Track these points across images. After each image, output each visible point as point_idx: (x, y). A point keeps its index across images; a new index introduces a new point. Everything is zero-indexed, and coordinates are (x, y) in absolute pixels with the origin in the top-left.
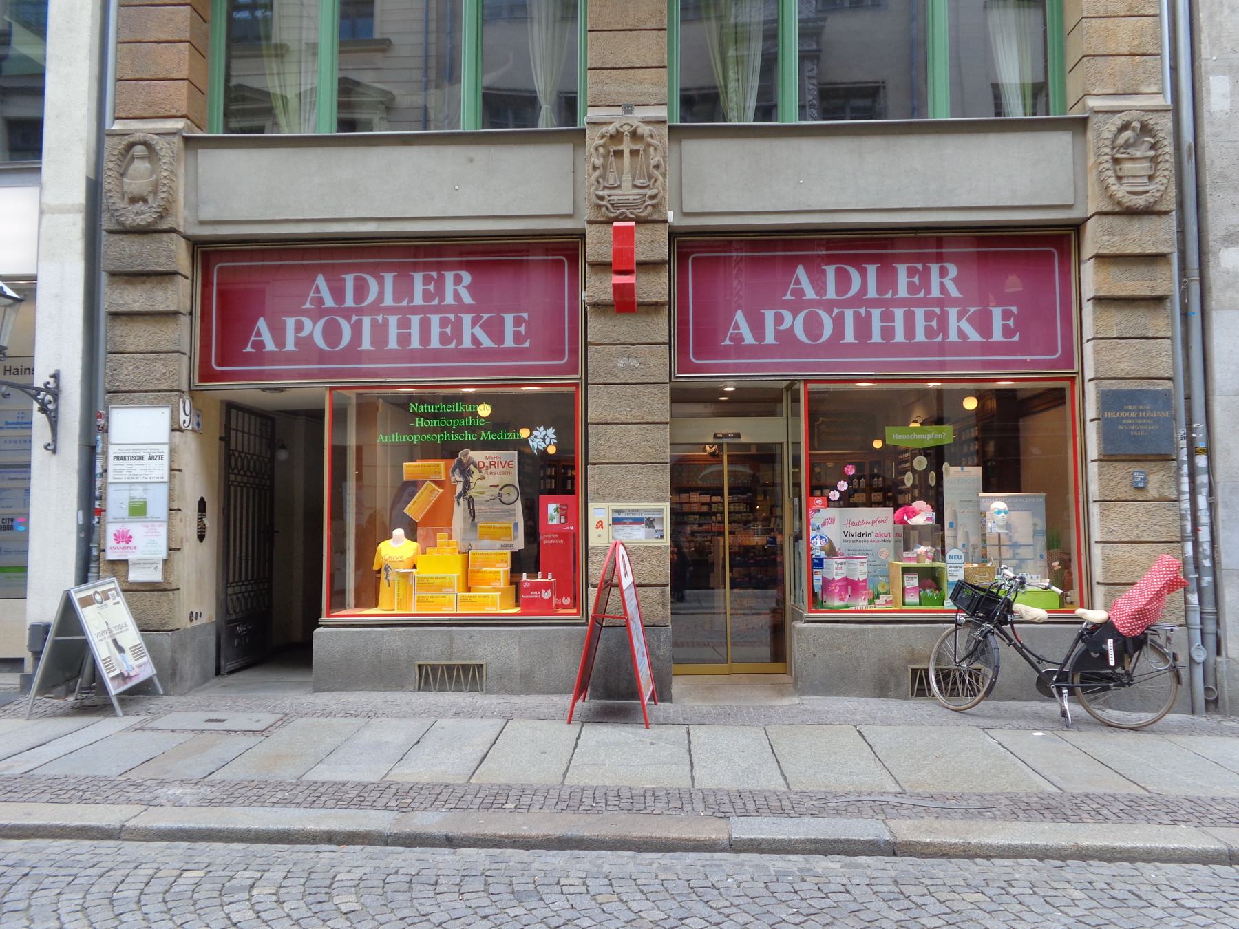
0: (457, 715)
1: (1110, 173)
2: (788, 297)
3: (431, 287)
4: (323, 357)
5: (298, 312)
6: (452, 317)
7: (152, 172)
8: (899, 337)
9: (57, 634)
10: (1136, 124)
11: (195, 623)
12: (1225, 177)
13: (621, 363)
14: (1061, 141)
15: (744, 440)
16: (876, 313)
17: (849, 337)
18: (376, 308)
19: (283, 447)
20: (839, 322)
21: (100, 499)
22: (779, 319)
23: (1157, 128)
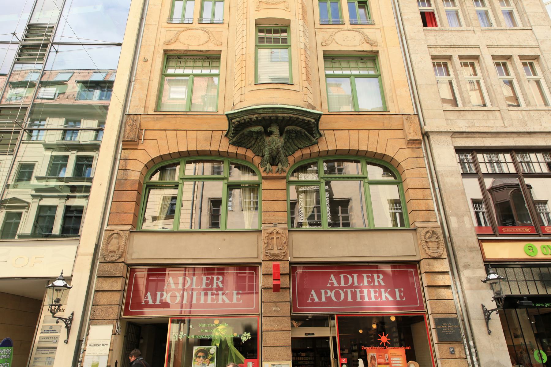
2: (329, 285)
5: (326, 288)
12: (460, 247)
13: (274, 309)
15: (316, 336)
16: (358, 291)
17: (350, 299)
19: (142, 338)
21: (81, 362)
22: (326, 293)
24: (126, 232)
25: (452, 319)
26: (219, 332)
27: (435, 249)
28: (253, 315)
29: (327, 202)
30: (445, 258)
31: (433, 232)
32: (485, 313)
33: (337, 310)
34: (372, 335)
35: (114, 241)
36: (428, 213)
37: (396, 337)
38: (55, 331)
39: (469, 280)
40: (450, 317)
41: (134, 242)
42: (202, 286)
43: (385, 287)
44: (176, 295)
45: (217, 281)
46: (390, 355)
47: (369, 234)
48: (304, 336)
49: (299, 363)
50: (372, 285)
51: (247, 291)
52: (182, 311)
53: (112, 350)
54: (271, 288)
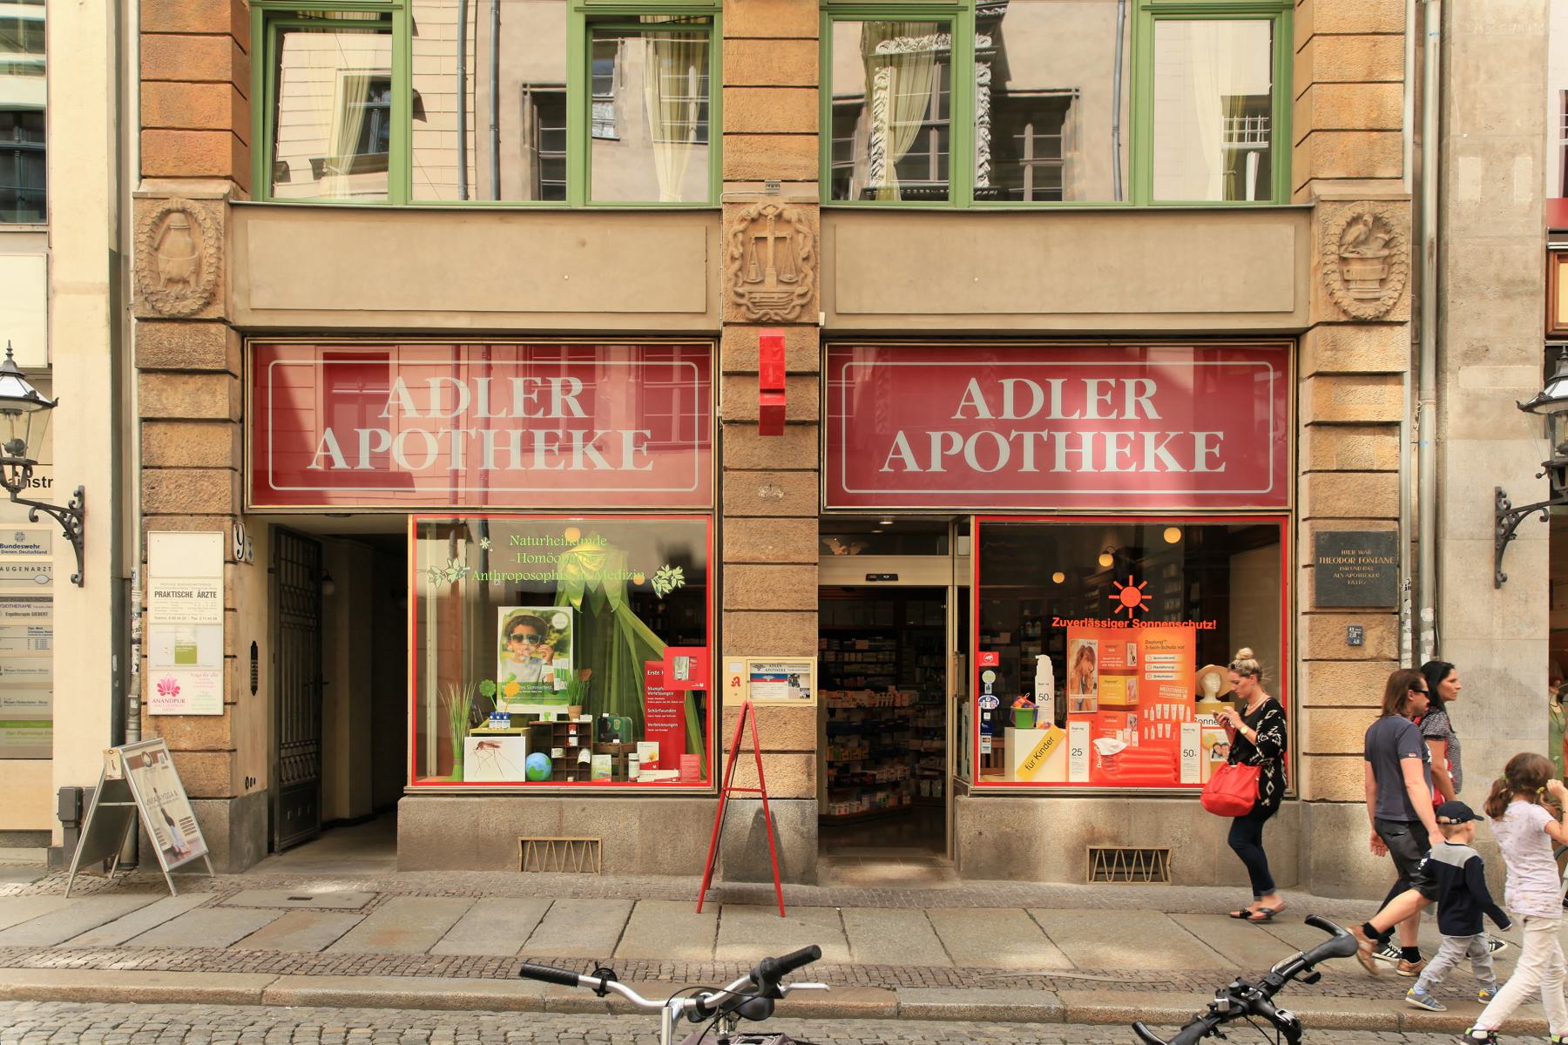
0: (575, 895)
1: (1336, 276)
2: (958, 416)
5: (946, 424)
9: (102, 799)
10: (1369, 219)
11: (252, 790)
12: (1468, 280)
13: (762, 492)
14: (1283, 232)
15: (901, 582)
16: (1061, 437)
17: (1029, 465)
19: (328, 578)
21: (139, 641)
22: (947, 443)
23: (1393, 222)
24: (213, 205)
25: (1378, 536)
26: (577, 563)
28: (693, 513)
29: (981, 107)
30: (1401, 324)
31: (1377, 219)
32: (1499, 520)
33: (975, 502)
34: (1094, 588)
35: (176, 241)
36: (1371, 144)
37: (1174, 596)
38: (34, 549)
39: (1473, 403)
40: (1373, 530)
41: (251, 246)
42: (511, 410)
43: (1161, 427)
44: (429, 440)
45: (564, 394)
46: (1143, 645)
47: (1128, 227)
48: (863, 582)
49: (847, 668)
50: (1113, 416)
51: (675, 439)
52: (456, 493)
53: (234, 610)
54: (752, 423)
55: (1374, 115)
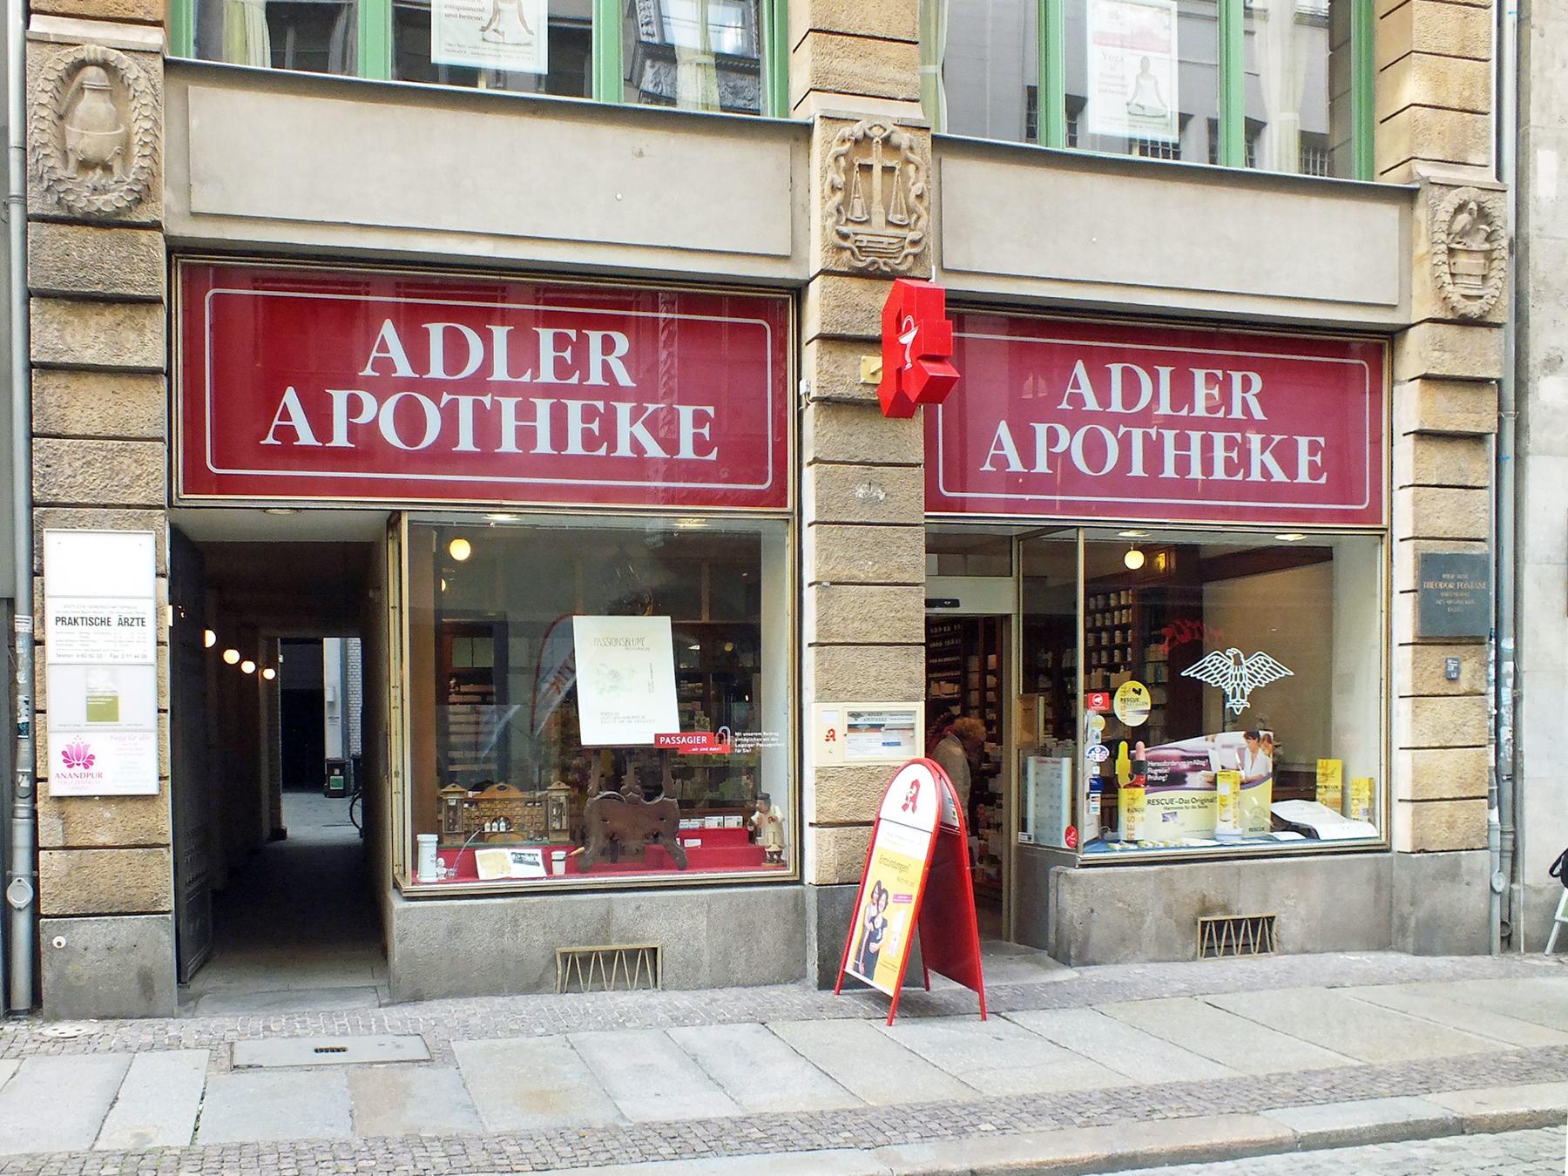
2: (1064, 405)
3: (567, 355)
4: (308, 456)
5: (348, 380)
6: (600, 405)
7: (119, 119)
8: (543, 445)
10: (1473, 205)
12: (1547, 285)
13: (861, 492)
14: (1386, 215)
15: (961, 610)
17: (1138, 470)
18: (479, 383)
20: (450, 416)
22: (354, 407)
24: (147, 59)
27: (1472, 286)
31: (1481, 209)
35: (92, 106)
40: (1467, 552)
43: (640, 395)
55: (1466, 93)
